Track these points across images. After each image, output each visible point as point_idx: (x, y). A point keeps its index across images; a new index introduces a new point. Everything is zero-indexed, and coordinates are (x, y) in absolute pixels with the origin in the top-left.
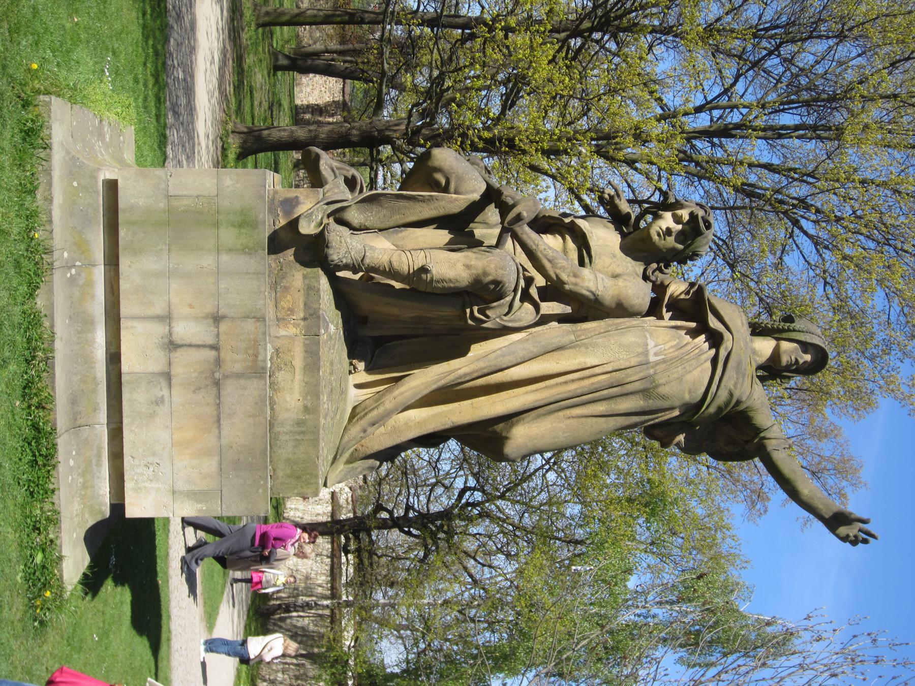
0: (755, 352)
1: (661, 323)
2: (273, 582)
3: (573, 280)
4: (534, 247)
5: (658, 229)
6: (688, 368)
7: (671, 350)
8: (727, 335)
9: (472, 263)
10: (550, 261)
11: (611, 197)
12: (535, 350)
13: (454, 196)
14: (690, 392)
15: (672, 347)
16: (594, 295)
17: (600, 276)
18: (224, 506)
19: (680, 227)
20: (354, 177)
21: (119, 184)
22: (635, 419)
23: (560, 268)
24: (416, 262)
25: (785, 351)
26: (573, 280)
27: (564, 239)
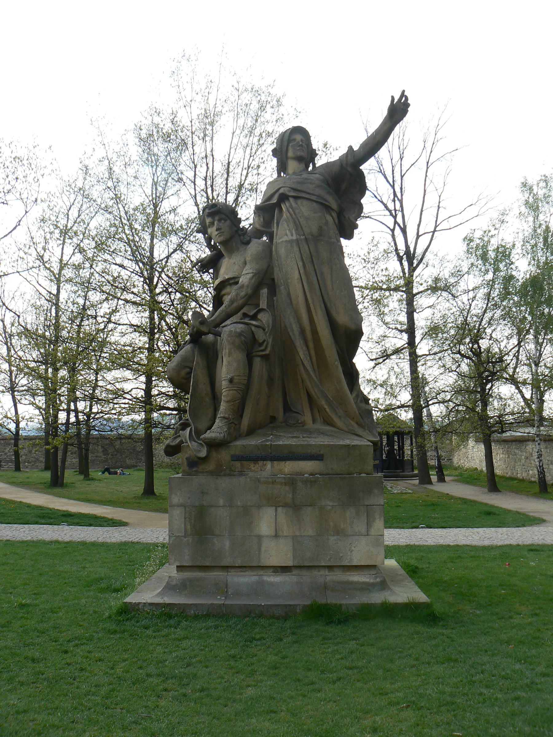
1: (275, 232)
6: (300, 215)
8: (281, 191)
15: (288, 226)
17: (244, 272)
26: (244, 289)
27: (224, 295)
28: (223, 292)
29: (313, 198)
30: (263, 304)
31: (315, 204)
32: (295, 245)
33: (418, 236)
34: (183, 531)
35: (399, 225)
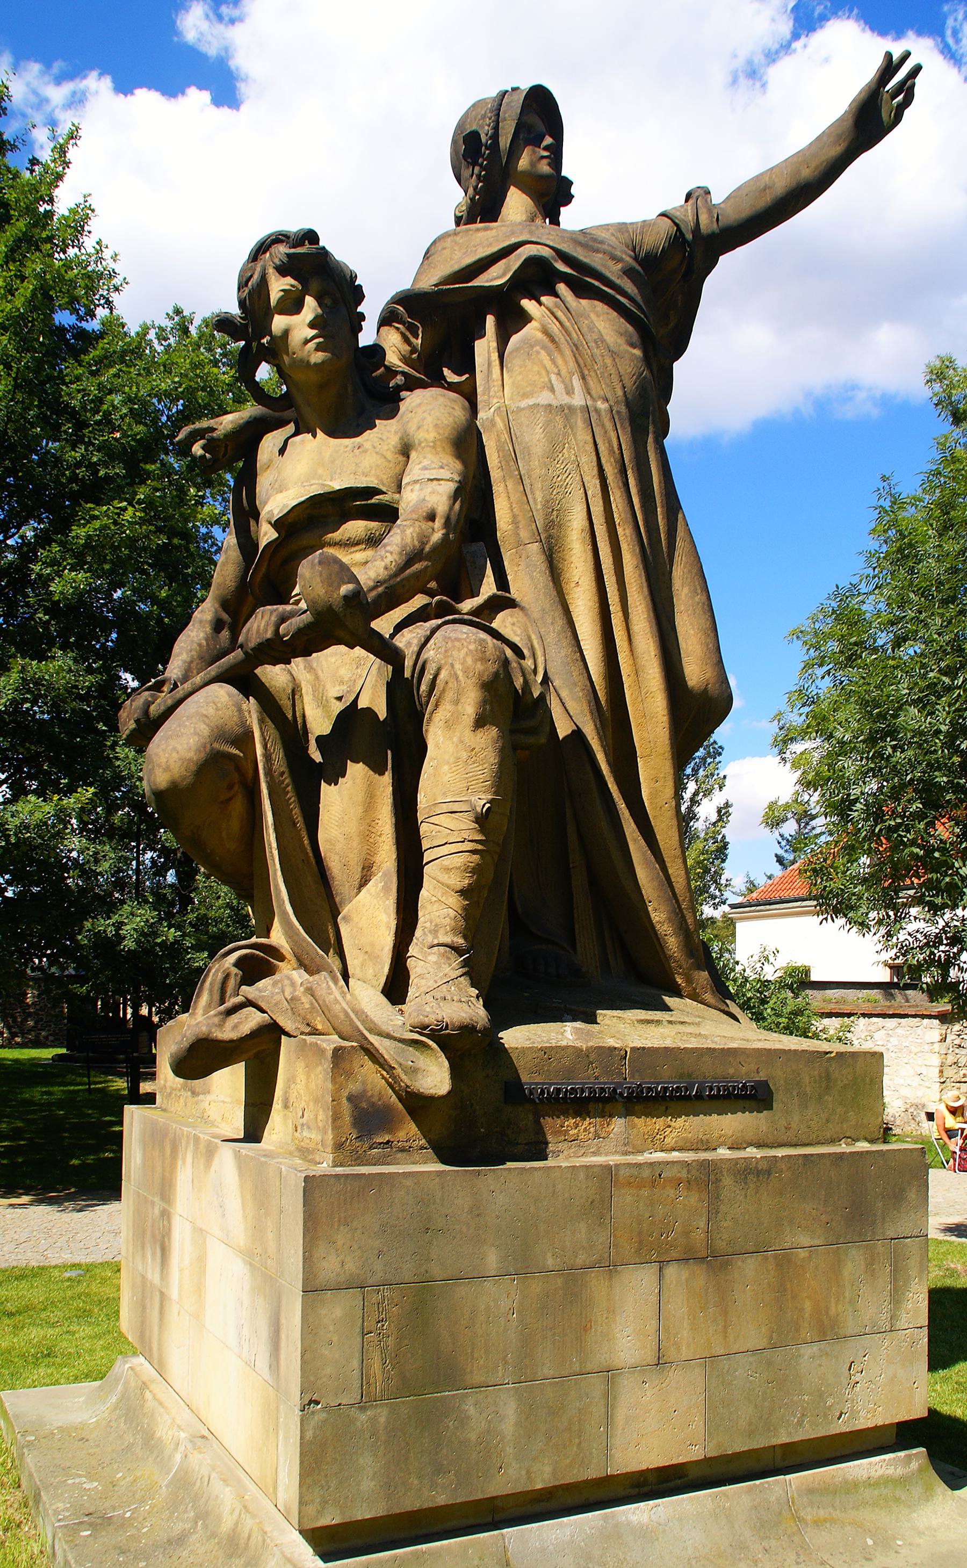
7: (560, 361)
15: (553, 361)
19: (309, 301)
24: (465, 835)
32: (580, 423)
34: (357, 1384)
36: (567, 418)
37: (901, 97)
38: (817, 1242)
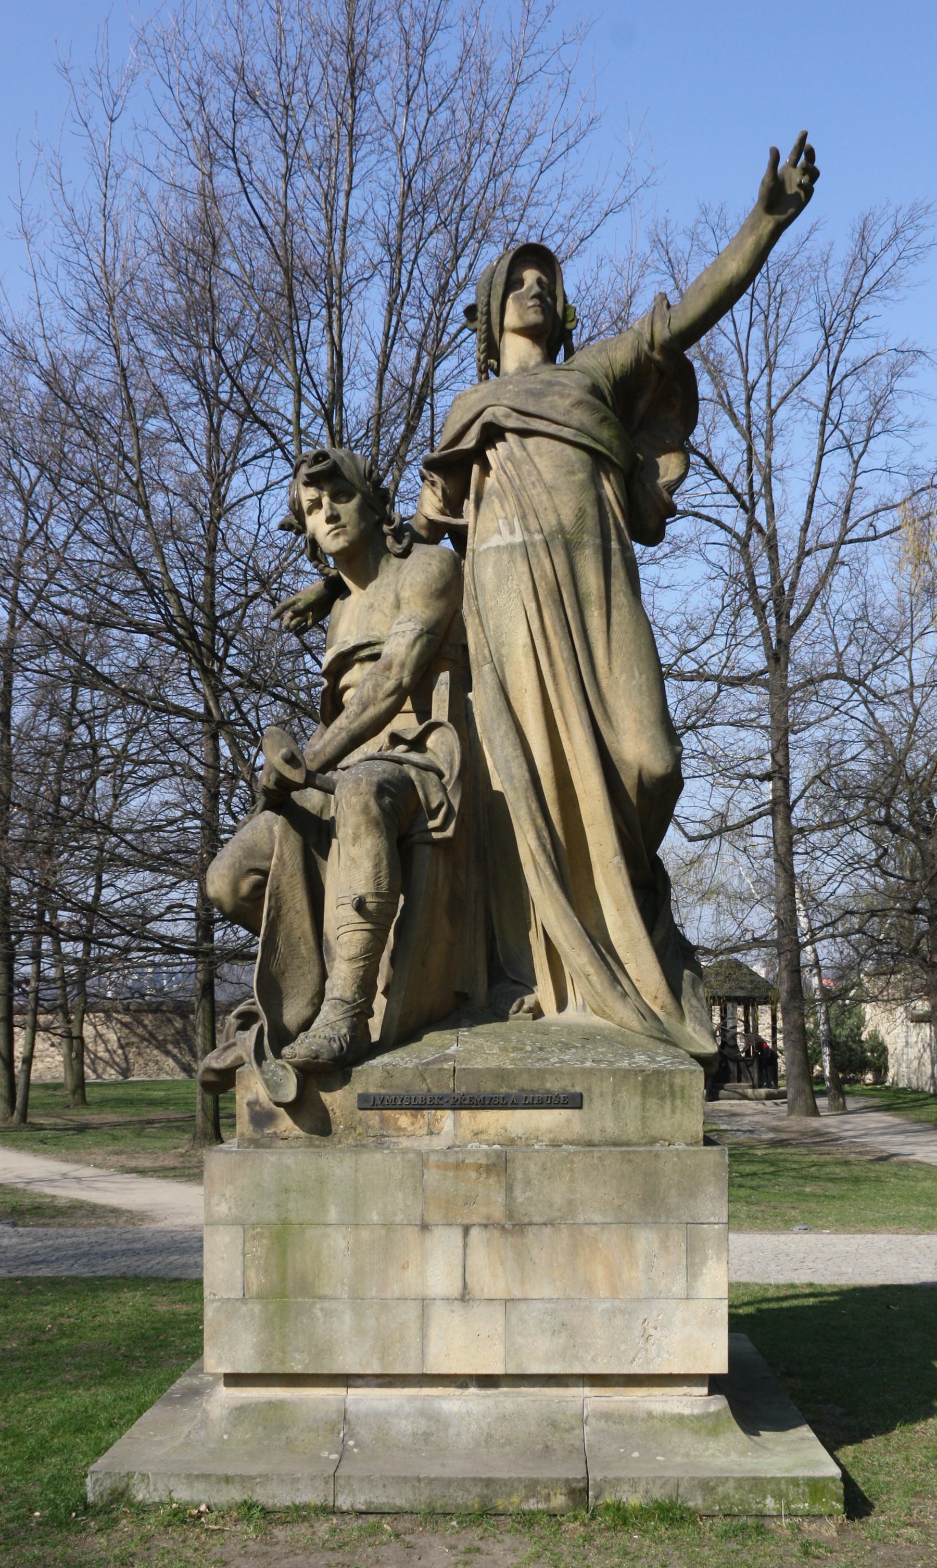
0: (523, 370)
1: (471, 526)
2: (715, 1156)
3: (395, 670)
4: (344, 734)
5: (329, 537)
6: (533, 478)
7: (507, 507)
8: (486, 417)
9: (350, 831)
10: (364, 709)
11: (296, 614)
12: (503, 727)
13: (274, 860)
14: (573, 473)
15: (502, 506)
16: (419, 636)
18: (712, 1220)
20: (239, 1016)
21: (228, 1371)
22: (616, 561)
23: (375, 691)
25: (520, 317)
26: (395, 670)
27: (347, 688)
28: (344, 682)
29: (566, 433)
30: (440, 709)
31: (569, 450)
33: (804, 553)
34: (240, 1286)
35: (760, 530)
36: (511, 555)
37: (803, 157)
38: (609, 1220)
